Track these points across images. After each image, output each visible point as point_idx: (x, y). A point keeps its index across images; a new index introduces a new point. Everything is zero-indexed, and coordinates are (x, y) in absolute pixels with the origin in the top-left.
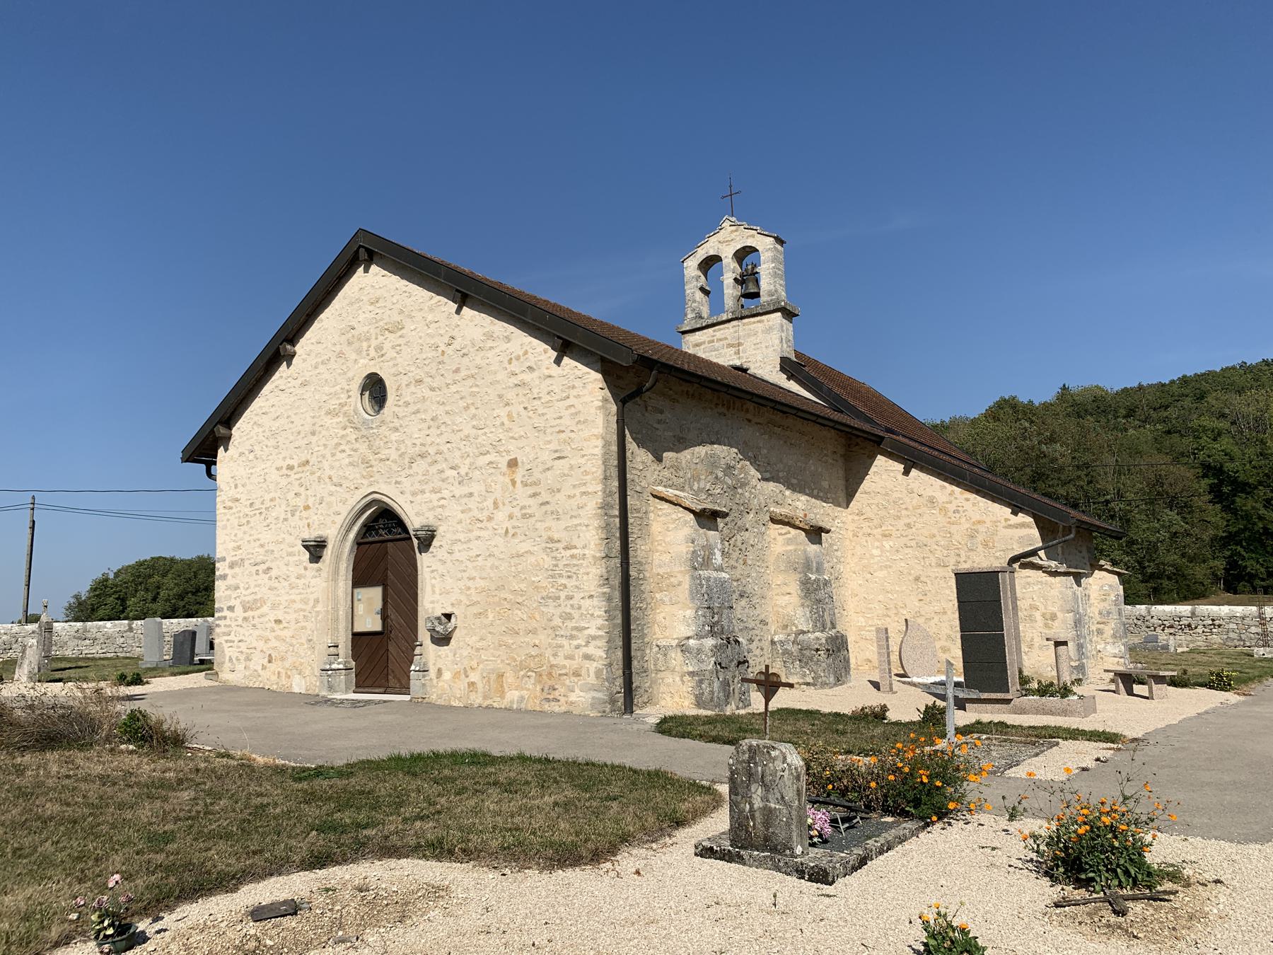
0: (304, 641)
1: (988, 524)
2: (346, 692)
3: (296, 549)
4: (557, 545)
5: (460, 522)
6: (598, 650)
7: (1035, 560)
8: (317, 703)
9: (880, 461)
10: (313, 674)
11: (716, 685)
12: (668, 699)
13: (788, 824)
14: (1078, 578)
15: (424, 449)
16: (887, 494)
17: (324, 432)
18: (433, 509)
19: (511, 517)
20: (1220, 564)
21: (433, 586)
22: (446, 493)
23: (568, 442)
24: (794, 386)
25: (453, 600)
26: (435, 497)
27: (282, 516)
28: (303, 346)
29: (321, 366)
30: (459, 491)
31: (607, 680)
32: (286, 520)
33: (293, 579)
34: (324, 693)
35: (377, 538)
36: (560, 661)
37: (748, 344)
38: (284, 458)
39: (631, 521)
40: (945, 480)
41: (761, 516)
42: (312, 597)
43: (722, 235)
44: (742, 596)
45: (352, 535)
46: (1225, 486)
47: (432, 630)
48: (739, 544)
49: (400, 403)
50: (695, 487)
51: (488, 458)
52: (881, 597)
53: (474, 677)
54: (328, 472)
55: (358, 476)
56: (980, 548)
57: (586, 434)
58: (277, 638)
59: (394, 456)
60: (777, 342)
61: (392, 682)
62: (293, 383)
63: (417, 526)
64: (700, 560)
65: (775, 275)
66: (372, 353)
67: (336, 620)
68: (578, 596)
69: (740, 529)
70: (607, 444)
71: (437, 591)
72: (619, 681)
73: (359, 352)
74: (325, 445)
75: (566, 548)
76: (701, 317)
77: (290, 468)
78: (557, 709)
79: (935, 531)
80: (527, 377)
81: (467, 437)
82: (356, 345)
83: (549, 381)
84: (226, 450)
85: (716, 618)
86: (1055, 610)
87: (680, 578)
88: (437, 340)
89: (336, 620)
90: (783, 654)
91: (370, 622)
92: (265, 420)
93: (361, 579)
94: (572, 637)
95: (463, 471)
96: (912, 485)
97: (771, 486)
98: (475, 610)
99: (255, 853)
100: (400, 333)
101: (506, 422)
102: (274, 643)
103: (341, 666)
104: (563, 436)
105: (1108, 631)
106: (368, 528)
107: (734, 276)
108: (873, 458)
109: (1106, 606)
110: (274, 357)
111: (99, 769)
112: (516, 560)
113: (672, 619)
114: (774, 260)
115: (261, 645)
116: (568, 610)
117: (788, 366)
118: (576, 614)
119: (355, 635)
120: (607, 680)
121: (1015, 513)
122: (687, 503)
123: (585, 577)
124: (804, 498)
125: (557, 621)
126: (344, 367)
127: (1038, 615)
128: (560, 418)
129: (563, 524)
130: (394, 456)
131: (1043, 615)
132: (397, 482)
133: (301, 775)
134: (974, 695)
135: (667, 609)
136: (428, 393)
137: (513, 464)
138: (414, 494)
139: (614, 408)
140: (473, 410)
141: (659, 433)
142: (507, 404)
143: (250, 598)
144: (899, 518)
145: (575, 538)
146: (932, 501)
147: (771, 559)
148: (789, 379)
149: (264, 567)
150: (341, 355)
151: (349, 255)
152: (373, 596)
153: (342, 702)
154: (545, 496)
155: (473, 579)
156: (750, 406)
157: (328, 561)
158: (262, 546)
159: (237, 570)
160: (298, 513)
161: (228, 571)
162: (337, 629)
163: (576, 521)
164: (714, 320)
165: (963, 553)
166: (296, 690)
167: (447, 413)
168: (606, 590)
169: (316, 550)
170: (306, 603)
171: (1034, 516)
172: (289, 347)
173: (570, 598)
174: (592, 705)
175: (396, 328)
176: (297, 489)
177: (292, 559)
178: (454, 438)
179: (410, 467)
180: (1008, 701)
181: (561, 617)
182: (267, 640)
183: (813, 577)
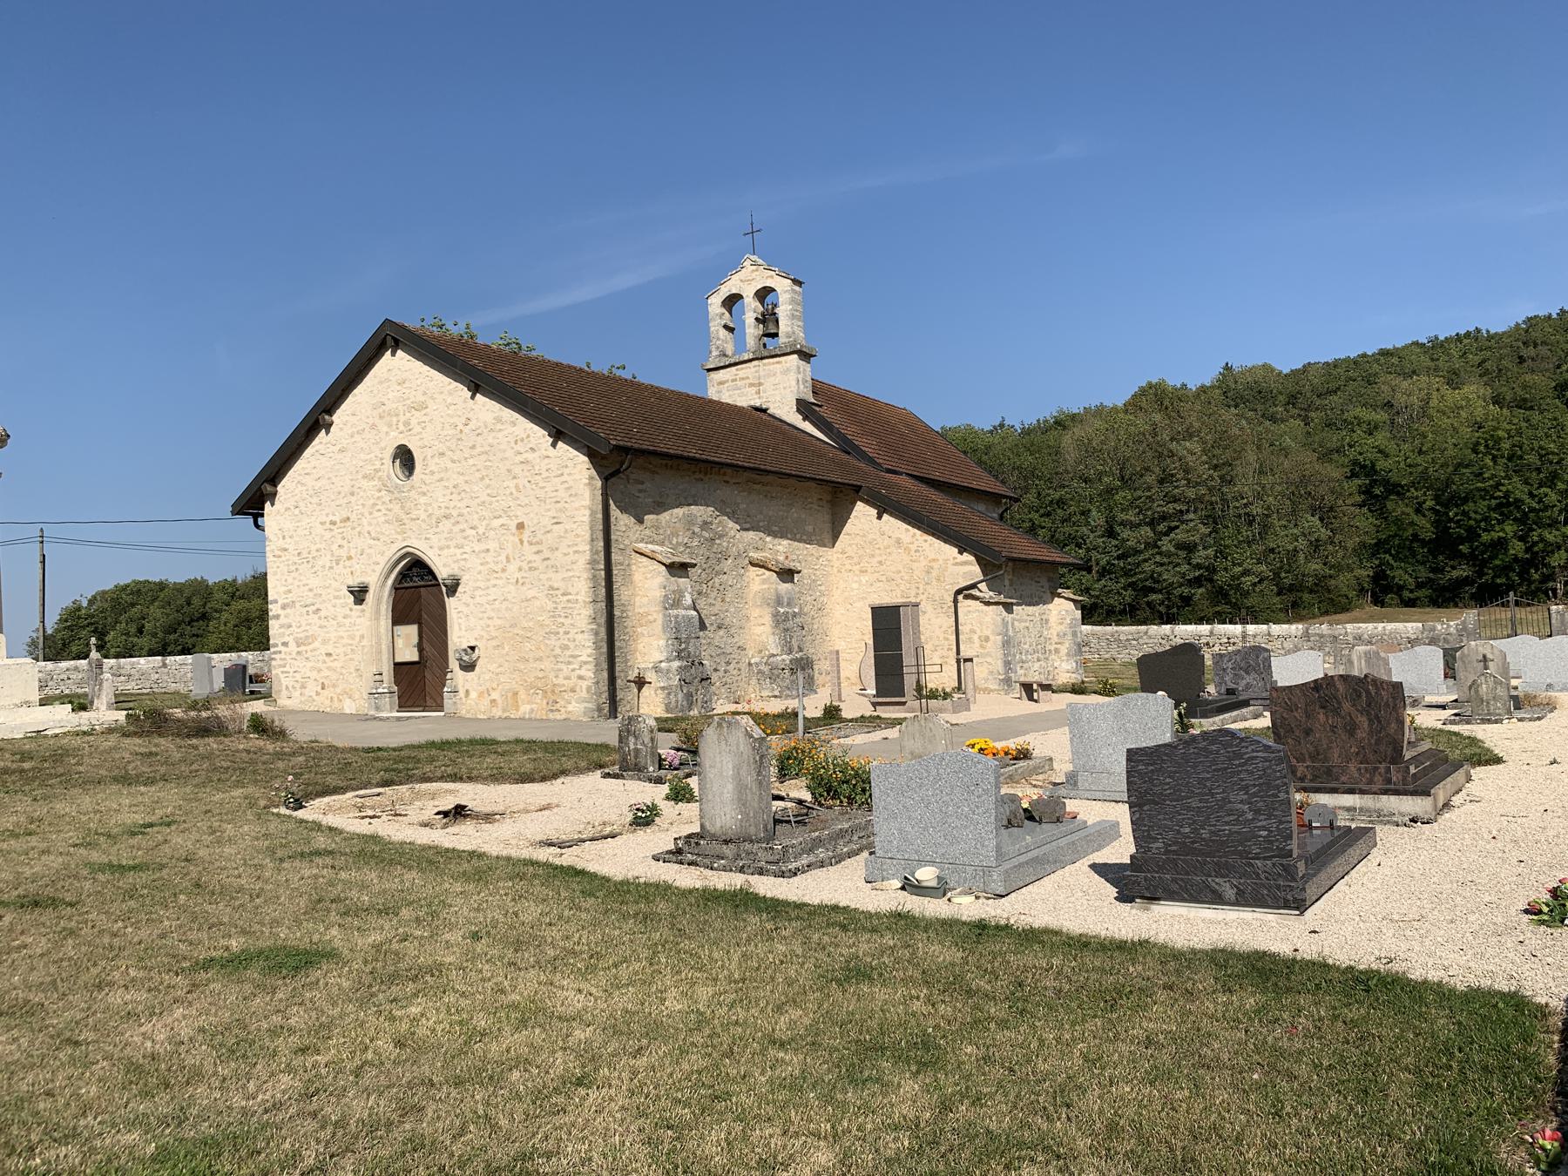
7: (974, 592)
9: (860, 506)
11: (680, 696)
14: (1008, 607)
20: (1365, 573)
22: (467, 549)
24: (808, 427)
28: (339, 417)
33: (340, 619)
34: (372, 712)
36: (560, 681)
37: (768, 384)
43: (742, 274)
45: (390, 582)
46: (1377, 489)
47: (460, 659)
51: (501, 521)
53: (495, 695)
54: (367, 528)
57: (576, 505)
59: (423, 516)
65: (793, 317)
66: (401, 427)
68: (573, 631)
69: (718, 574)
70: (593, 513)
72: (606, 695)
73: (390, 425)
80: (530, 456)
86: (988, 633)
88: (455, 420)
91: (408, 653)
92: (308, 480)
93: (399, 618)
98: (494, 643)
105: (1064, 650)
106: (403, 576)
110: (314, 424)
113: (649, 649)
114: (792, 301)
115: (314, 674)
117: (803, 407)
118: (572, 645)
119: (396, 664)
122: (660, 558)
124: (785, 542)
125: (558, 651)
127: (975, 637)
130: (423, 516)
133: (369, 750)
135: (646, 640)
136: (449, 465)
137: (521, 526)
138: (441, 549)
139: (599, 483)
146: (898, 541)
150: (373, 426)
154: (547, 554)
161: (280, 612)
162: (380, 660)
169: (359, 594)
175: (422, 407)
176: (340, 542)
180: (904, 703)
182: (320, 671)
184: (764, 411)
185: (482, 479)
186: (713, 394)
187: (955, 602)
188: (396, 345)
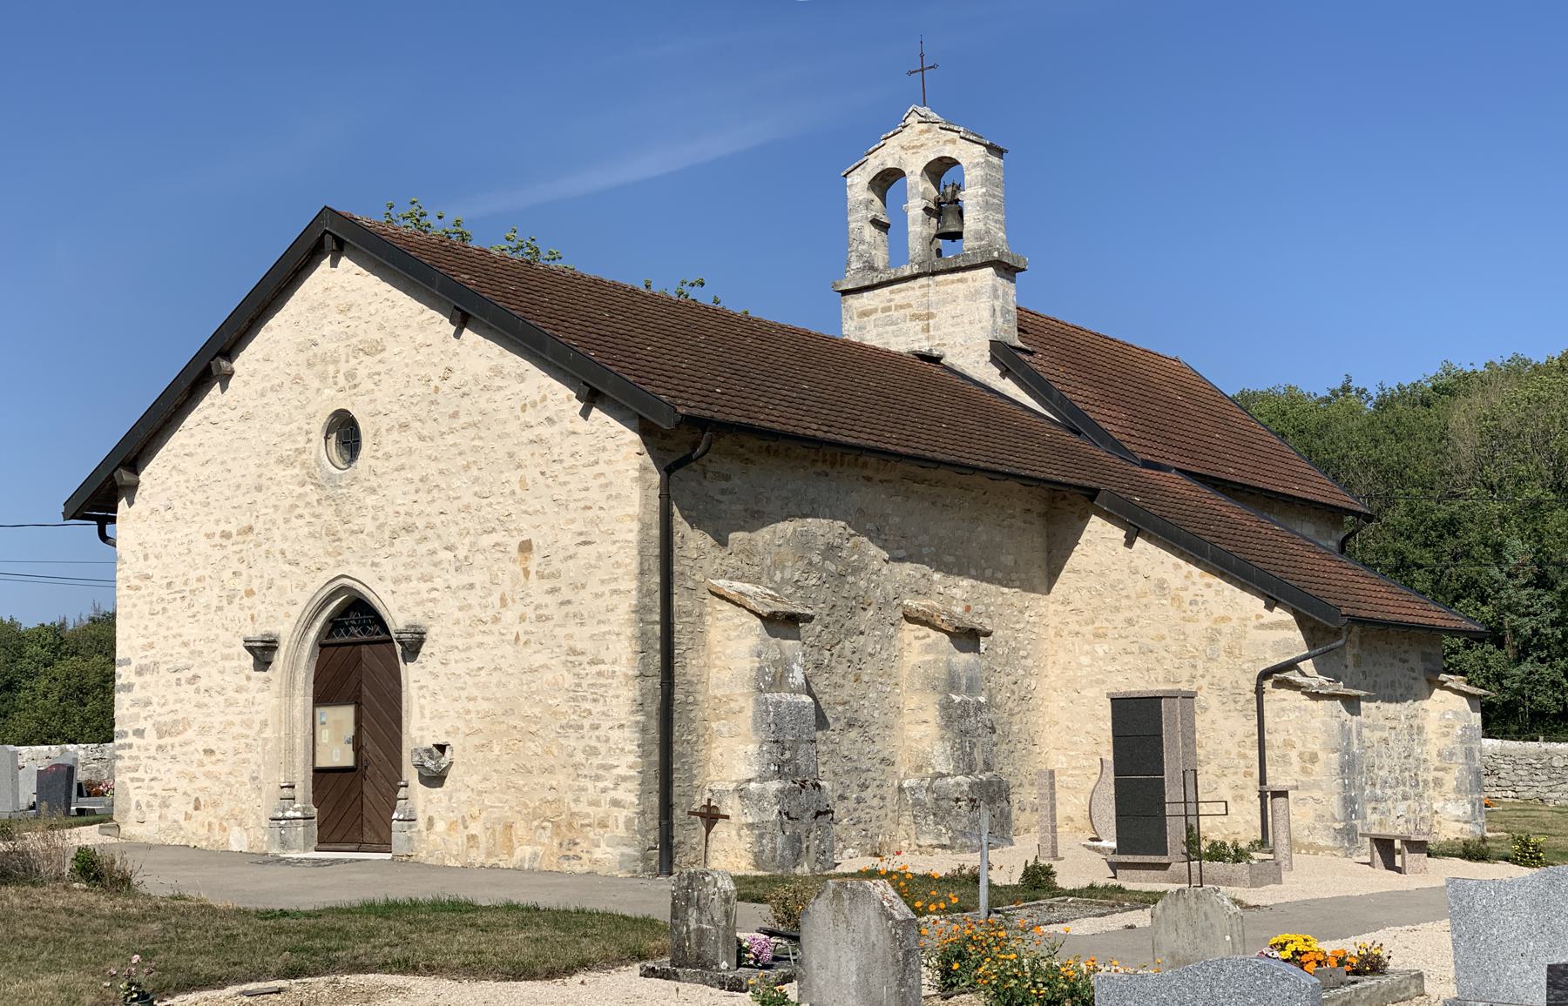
0: (246, 778)
1: (1235, 622)
2: (306, 850)
3: (234, 651)
4: (580, 658)
5: (457, 622)
6: (629, 794)
7: (1293, 676)
8: (266, 862)
9: (1094, 518)
10: (259, 825)
11: (780, 840)
12: (721, 858)
13: (716, 942)
14: (1352, 704)
15: (410, 520)
16: (1102, 574)
17: (274, 488)
18: (421, 603)
19: (522, 619)
21: (422, 707)
22: (438, 583)
23: (595, 522)
25: (448, 726)
26: (424, 586)
27: (215, 603)
28: (245, 363)
29: (269, 394)
30: (456, 580)
31: (639, 832)
32: (220, 608)
33: (230, 693)
34: (275, 850)
35: (347, 639)
36: (583, 808)
37: (943, 315)
38: (217, 522)
39: (678, 627)
40: (1181, 555)
41: (887, 612)
42: (258, 718)
43: (906, 137)
44: (850, 726)
45: (313, 634)
48: (847, 652)
49: (379, 454)
50: (778, 577)
51: (495, 538)
52: (1090, 727)
53: (475, 828)
54: (280, 545)
55: (321, 551)
56: (1223, 657)
57: (619, 512)
58: (208, 775)
59: (370, 526)
60: (986, 314)
61: (369, 835)
62: (230, 414)
63: (401, 627)
64: (771, 679)
65: (987, 206)
66: (342, 381)
67: (291, 750)
68: (605, 725)
69: (849, 633)
70: (645, 528)
71: (427, 713)
73: (323, 378)
74: (276, 507)
75: (592, 663)
76: (872, 268)
77: (226, 535)
78: (578, 869)
79: (1166, 632)
80: (546, 431)
81: (468, 506)
82: (319, 368)
83: (572, 439)
84: (131, 503)
85: (788, 755)
86: (1315, 747)
87: (742, 702)
89: (291, 750)
90: (914, 805)
91: (338, 755)
92: (187, 464)
93: (325, 695)
94: (598, 778)
95: (462, 552)
96: (1137, 562)
97: (908, 568)
98: (477, 740)
99: (235, 964)
100: (379, 357)
101: (518, 491)
102: (203, 782)
103: (298, 814)
104: (589, 513)
105: (1450, 781)
106: (335, 624)
107: (924, 203)
108: (1084, 519)
109: (1447, 743)
110: (203, 374)
111: (60, 903)
112: (529, 677)
113: (730, 759)
114: (986, 181)
115: (183, 785)
116: (593, 743)
117: (1002, 354)
118: (602, 748)
119: (318, 772)
120: (639, 832)
121: (1269, 607)
122: (752, 604)
123: (615, 701)
124: (966, 583)
125: (580, 757)
126: (302, 398)
127: (1294, 755)
128: (587, 489)
129: (589, 630)
130: (370, 526)
131: (1301, 755)
132: (373, 564)
134: (1124, 859)
136: (416, 444)
137: (526, 547)
138: (396, 581)
139: (656, 478)
140: (474, 471)
141: (723, 507)
142: (519, 466)
143: (168, 718)
144: (1117, 609)
145: (603, 650)
146: (1161, 586)
147: (905, 672)
148: (1003, 375)
149: (188, 674)
150: (297, 380)
151: (313, 241)
152: (341, 719)
153: (300, 861)
154: (566, 593)
155: (474, 699)
156: (872, 460)
157: (279, 669)
158: (185, 644)
159: (147, 677)
160: (237, 600)
161: (134, 679)
163: (604, 628)
164: (890, 274)
165: (1200, 664)
166: (235, 847)
167: (441, 472)
168: (640, 718)
169: (263, 653)
170: (249, 727)
171: (1295, 613)
172: (224, 363)
173: (596, 727)
174: (621, 863)
175: (374, 349)
176: (236, 566)
177: (228, 664)
178: (451, 507)
179: (392, 545)
180: (1165, 866)
181: (584, 751)
182: (193, 778)
183: (957, 699)
184: (936, 360)
185: (467, 467)
186: (851, 330)
187: (1259, 692)
188: (340, 249)
